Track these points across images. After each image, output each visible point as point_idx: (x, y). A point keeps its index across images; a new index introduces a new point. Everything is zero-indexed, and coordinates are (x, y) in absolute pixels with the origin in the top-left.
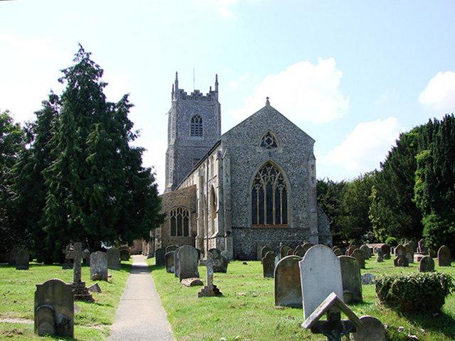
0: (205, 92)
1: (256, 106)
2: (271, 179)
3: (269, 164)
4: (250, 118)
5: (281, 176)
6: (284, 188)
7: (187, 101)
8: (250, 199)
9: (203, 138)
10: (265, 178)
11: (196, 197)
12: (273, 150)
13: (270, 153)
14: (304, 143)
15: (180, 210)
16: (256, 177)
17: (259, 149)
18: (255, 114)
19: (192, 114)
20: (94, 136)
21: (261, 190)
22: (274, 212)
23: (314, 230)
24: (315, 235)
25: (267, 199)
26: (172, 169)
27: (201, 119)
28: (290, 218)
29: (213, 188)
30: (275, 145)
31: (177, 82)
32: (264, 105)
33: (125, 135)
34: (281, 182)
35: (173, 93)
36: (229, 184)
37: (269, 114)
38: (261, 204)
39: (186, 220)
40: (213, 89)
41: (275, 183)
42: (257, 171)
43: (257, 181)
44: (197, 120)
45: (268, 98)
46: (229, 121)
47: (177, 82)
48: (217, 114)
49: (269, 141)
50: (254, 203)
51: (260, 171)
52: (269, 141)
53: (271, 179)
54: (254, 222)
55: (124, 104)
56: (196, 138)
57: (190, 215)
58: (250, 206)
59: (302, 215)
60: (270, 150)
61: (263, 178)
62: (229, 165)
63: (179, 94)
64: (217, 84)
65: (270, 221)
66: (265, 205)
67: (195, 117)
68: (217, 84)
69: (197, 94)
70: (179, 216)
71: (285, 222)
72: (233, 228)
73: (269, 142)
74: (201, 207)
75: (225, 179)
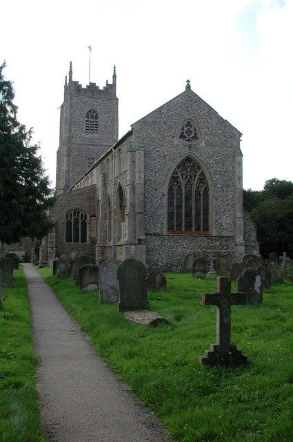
0: (101, 86)
1: (172, 91)
2: (191, 177)
3: (188, 159)
5: (203, 174)
8: (165, 200)
12: (193, 143)
14: (229, 136)
15: (76, 211)
16: (173, 174)
17: (177, 141)
19: (88, 109)
21: (179, 189)
22: (194, 215)
25: (186, 202)
26: (65, 168)
27: (97, 115)
28: (212, 223)
29: (120, 189)
30: (195, 137)
31: (71, 73)
32: (184, 89)
35: (65, 87)
37: (189, 100)
39: (84, 224)
40: (111, 82)
44: (92, 115)
45: (188, 81)
46: (127, 117)
47: (71, 73)
49: (189, 132)
51: (178, 167)
52: (189, 132)
53: (191, 177)
54: (170, 228)
56: (89, 136)
58: (165, 209)
59: (226, 221)
60: (190, 143)
62: (142, 159)
63: (73, 89)
64: (115, 77)
65: (188, 227)
67: (90, 112)
68: (115, 77)
69: (92, 86)
70: (76, 220)
71: (206, 228)
74: (104, 209)
75: (137, 175)
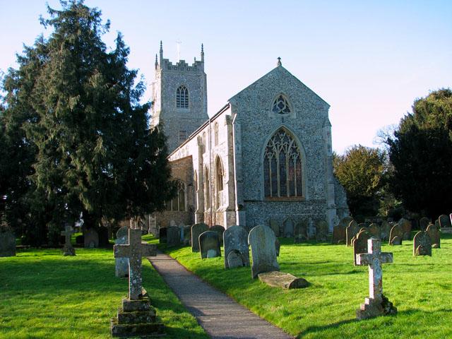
3: (281, 131)
4: (261, 80)
5: (295, 144)
6: (274, 156)
7: (172, 72)
8: (262, 169)
9: (189, 110)
10: (278, 146)
11: (191, 168)
12: (285, 115)
13: (283, 119)
14: (319, 107)
17: (271, 114)
18: (266, 76)
19: (178, 85)
20: (95, 80)
23: (331, 202)
24: (333, 207)
28: (305, 190)
30: (287, 110)
31: (161, 51)
33: (127, 92)
34: (294, 150)
36: (240, 152)
38: (274, 175)
41: (289, 151)
42: (269, 138)
43: (269, 149)
45: (279, 58)
47: (161, 51)
48: (202, 85)
49: (281, 106)
50: (267, 174)
51: (273, 138)
54: (267, 195)
55: (122, 50)
56: (181, 110)
57: (186, 188)
59: (318, 187)
61: (276, 145)
64: (203, 54)
65: (284, 193)
66: (278, 175)
68: (203, 54)
69: (182, 64)
71: (300, 194)
72: (245, 201)
73: (282, 106)
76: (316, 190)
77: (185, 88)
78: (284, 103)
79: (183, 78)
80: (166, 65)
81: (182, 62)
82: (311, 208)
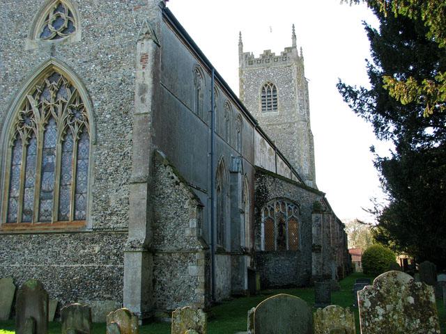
7: (255, 67)
9: (277, 113)
13: (53, 48)
19: (262, 82)
31: (241, 44)
47: (241, 44)
56: (267, 114)
69: (268, 56)
76: (113, 203)
77: (272, 85)
78: (64, 15)
79: (268, 72)
80: (247, 59)
81: (267, 52)
82: (97, 249)
